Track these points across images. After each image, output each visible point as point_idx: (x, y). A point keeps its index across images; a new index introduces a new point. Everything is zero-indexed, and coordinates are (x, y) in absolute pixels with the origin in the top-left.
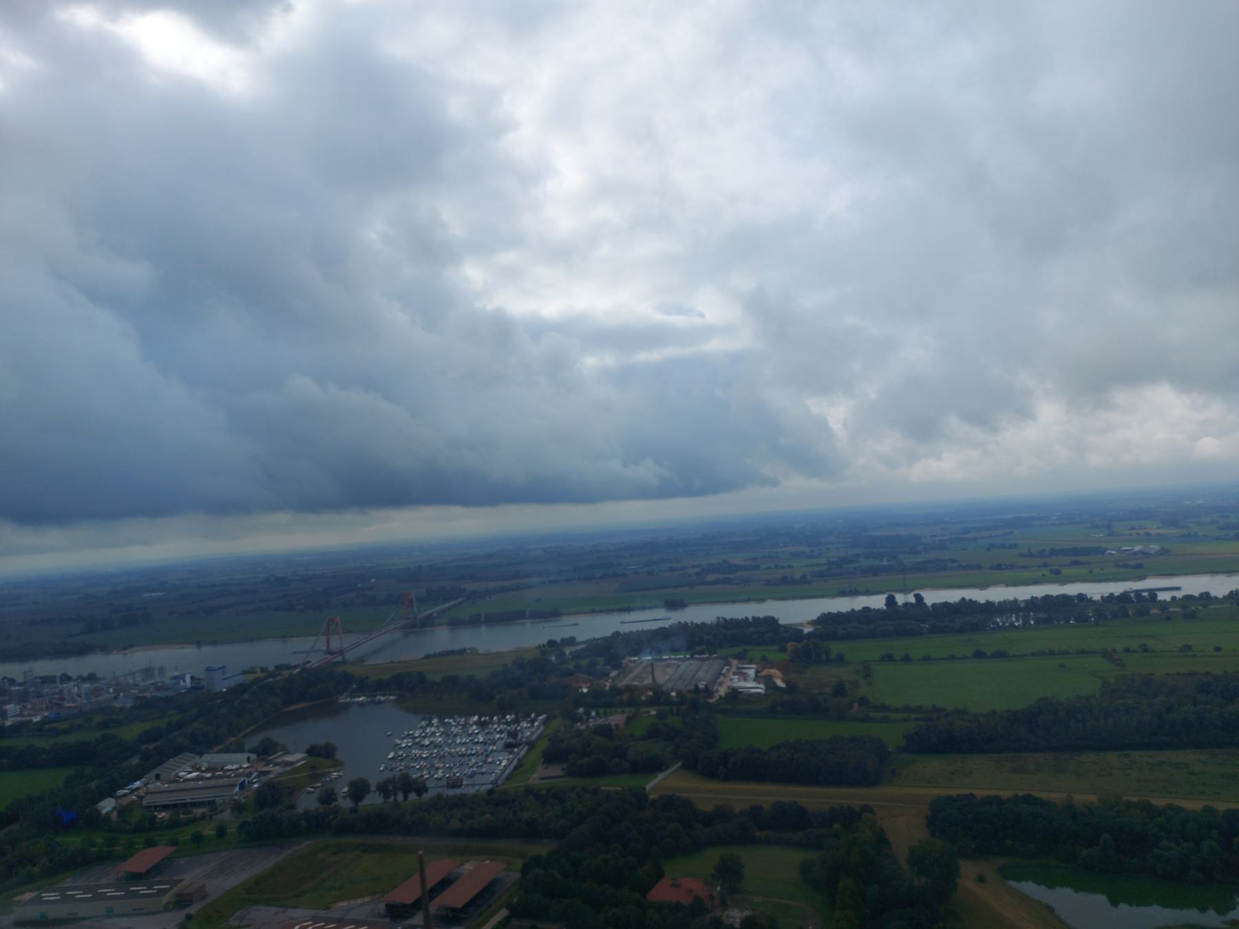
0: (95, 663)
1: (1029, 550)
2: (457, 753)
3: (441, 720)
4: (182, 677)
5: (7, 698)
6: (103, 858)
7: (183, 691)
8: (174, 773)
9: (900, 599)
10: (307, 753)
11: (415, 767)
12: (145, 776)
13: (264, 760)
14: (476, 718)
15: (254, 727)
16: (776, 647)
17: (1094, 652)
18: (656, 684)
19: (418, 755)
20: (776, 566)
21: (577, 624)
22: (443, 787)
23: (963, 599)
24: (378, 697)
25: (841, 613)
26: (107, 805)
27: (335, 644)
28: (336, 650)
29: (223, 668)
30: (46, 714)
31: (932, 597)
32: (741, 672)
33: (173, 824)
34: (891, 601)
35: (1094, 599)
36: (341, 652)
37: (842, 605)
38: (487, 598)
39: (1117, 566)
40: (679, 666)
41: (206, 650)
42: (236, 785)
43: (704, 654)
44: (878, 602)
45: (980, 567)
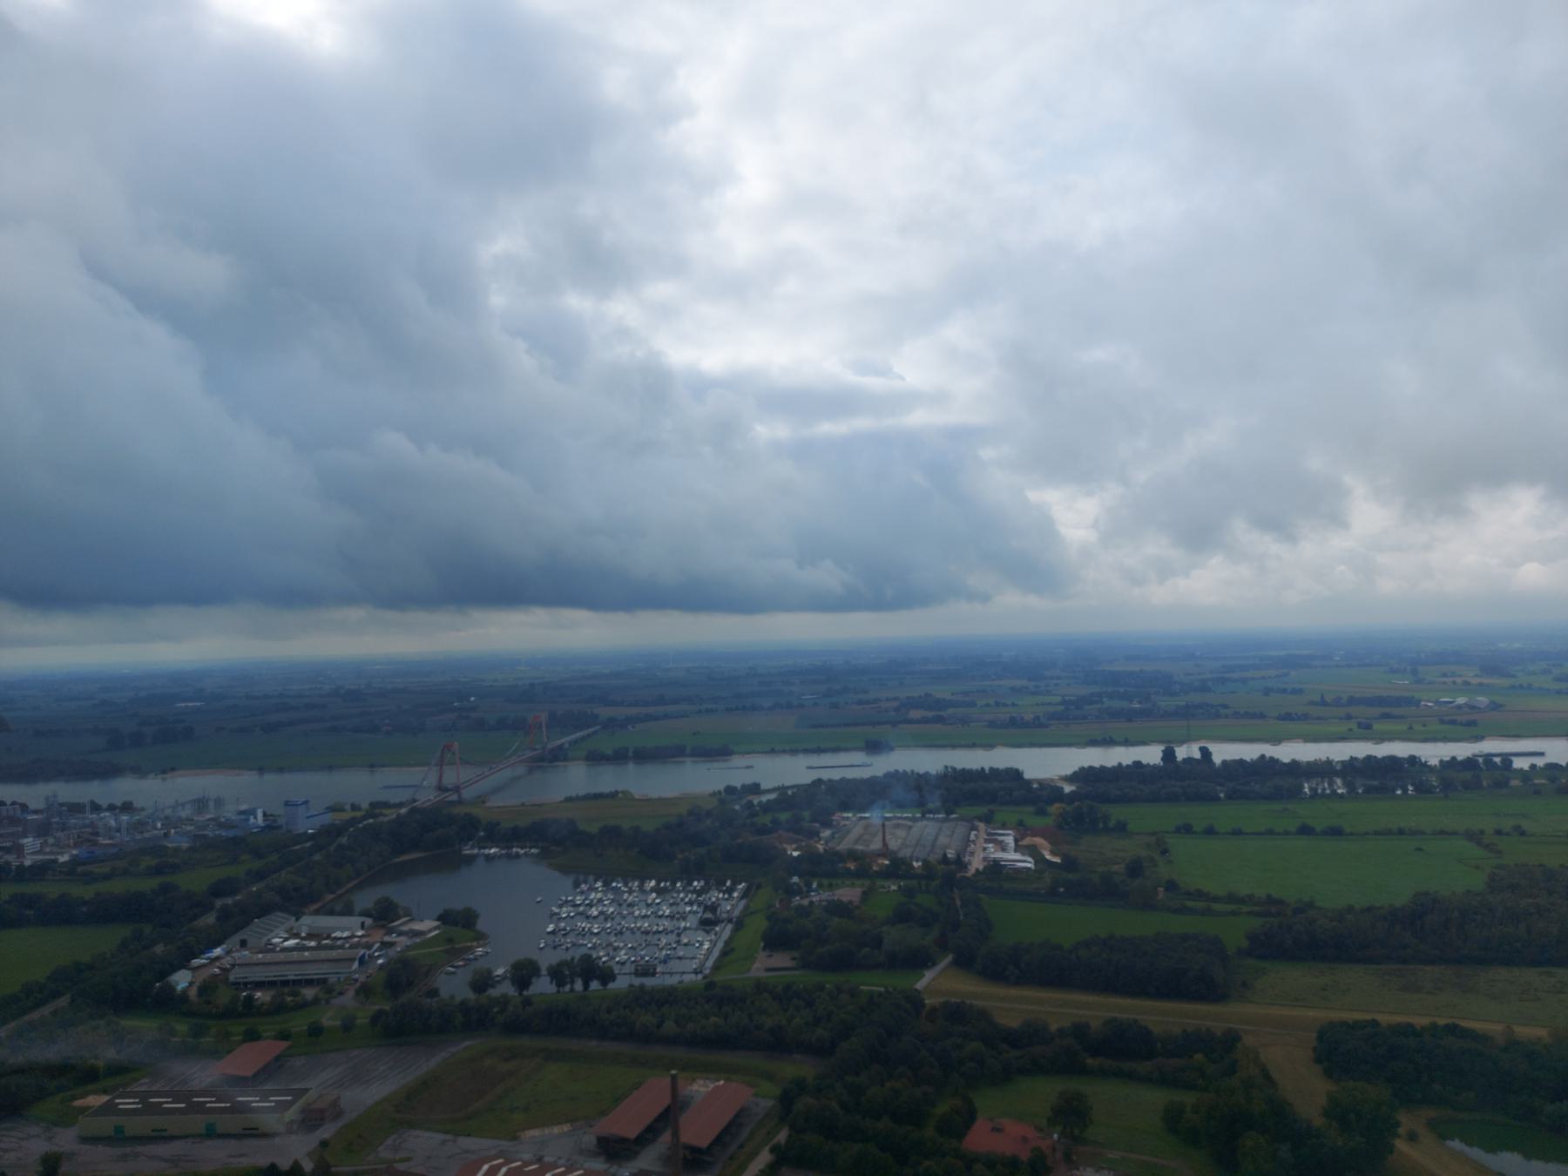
0: (124, 788)
1: (1322, 697)
2: (639, 929)
4: (253, 812)
5: (20, 829)
7: (255, 830)
8: (265, 940)
9: (1181, 753)
10: (438, 919)
11: (586, 945)
12: (227, 942)
13: (383, 927)
14: (653, 883)
15: (355, 882)
16: (1031, 809)
17: (1455, 833)
18: (887, 849)
19: (586, 929)
20: (997, 704)
21: (751, 767)
22: (630, 974)
24: (514, 850)
26: (181, 980)
27: (450, 778)
28: (450, 786)
29: (306, 802)
30: (75, 852)
31: (1222, 753)
32: (996, 839)
33: (277, 1009)
34: (1169, 755)
35: (1429, 764)
36: (457, 789)
38: (630, 727)
39: (1442, 722)
40: (910, 827)
41: (270, 778)
42: (353, 960)
43: (939, 813)
44: (1151, 755)
45: (1262, 716)
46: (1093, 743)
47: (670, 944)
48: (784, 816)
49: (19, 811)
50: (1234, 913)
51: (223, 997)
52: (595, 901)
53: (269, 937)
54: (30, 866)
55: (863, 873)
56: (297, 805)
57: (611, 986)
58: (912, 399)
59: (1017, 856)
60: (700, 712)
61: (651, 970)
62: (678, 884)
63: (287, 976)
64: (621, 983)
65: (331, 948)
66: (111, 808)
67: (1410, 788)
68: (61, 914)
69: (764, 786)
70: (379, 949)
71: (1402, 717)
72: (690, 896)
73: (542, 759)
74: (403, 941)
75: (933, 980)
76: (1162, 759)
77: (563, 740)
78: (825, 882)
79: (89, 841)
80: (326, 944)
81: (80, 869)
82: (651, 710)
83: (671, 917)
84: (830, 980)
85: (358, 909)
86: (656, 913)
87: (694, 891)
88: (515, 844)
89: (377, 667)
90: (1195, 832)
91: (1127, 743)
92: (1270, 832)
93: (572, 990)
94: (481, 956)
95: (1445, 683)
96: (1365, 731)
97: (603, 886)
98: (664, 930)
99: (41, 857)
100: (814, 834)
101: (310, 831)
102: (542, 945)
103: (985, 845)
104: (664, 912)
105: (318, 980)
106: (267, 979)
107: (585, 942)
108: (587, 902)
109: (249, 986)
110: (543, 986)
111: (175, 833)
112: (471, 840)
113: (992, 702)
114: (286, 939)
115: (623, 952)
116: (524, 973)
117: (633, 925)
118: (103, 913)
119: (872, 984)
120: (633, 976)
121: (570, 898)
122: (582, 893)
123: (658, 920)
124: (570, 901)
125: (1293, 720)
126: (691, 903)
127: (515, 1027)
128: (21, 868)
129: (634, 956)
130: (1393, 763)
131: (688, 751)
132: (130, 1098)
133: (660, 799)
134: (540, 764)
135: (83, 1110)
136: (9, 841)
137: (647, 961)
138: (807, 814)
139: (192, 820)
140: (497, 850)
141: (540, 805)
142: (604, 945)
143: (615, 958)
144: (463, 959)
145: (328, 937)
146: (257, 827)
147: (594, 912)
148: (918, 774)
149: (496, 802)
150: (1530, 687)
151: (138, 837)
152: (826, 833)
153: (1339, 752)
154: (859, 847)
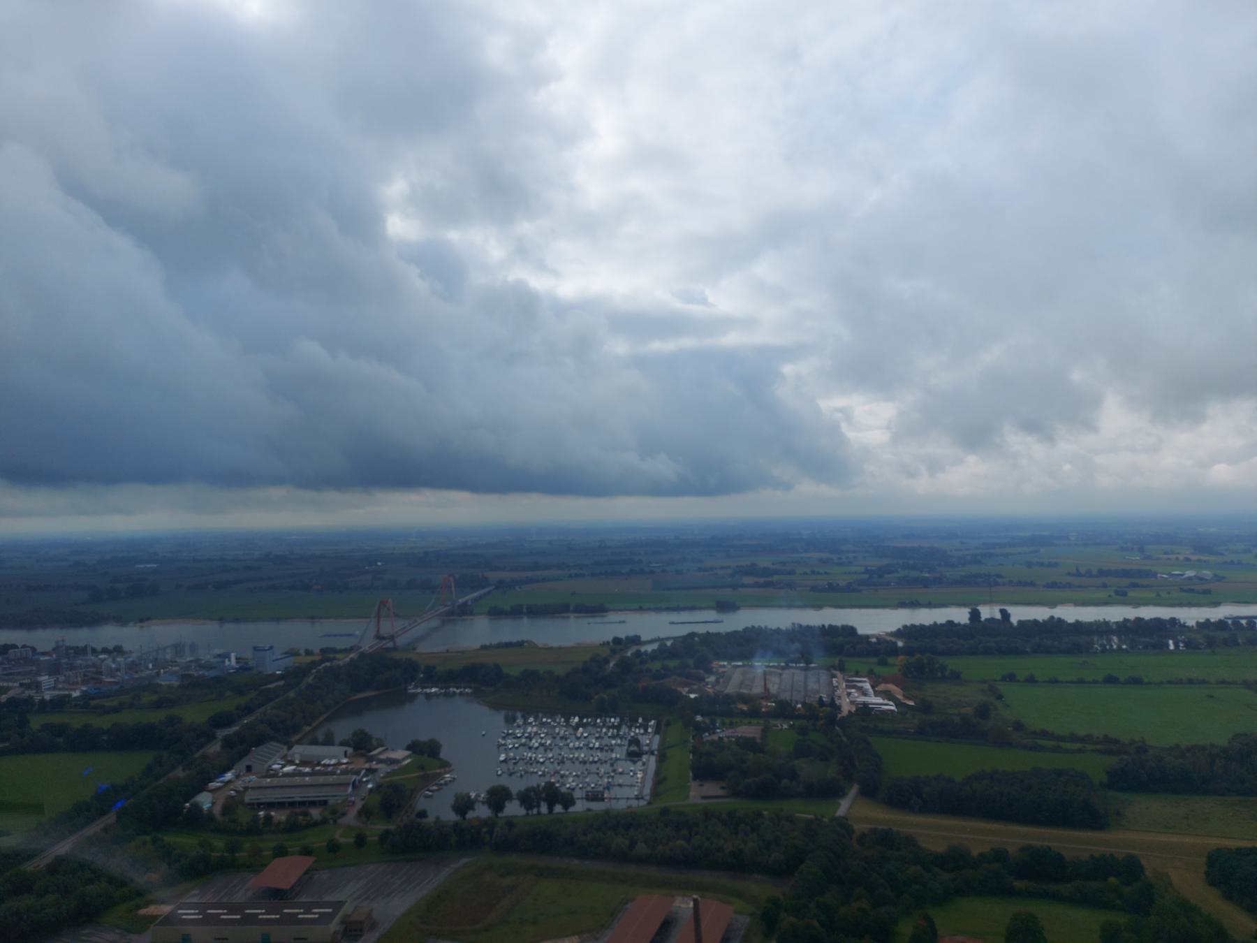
0: (108, 635)
1: (1077, 569)
2: (577, 759)
3: (536, 718)
4: (227, 656)
5: (34, 668)
6: (227, 866)
7: (232, 671)
8: (266, 766)
9: (986, 612)
10: (408, 748)
11: (536, 773)
12: (234, 767)
13: (362, 755)
14: (577, 719)
15: (324, 716)
16: (875, 660)
17: (1235, 683)
18: (769, 692)
19: (533, 759)
20: (813, 572)
21: (624, 622)
22: (582, 798)
23: (1052, 617)
24: (451, 689)
25: (924, 626)
26: (205, 800)
27: (386, 628)
28: (386, 635)
29: (271, 648)
30: (84, 688)
31: (1018, 614)
32: (855, 686)
33: (292, 827)
34: (975, 615)
35: (1187, 624)
36: (392, 638)
37: (926, 617)
38: (517, 588)
39: (1182, 590)
40: (780, 675)
41: (229, 627)
42: (347, 785)
43: (800, 663)
44: (960, 615)
45: (1032, 584)
46: (903, 605)
47: (608, 773)
48: (672, 664)
49: (30, 653)
50: (1080, 751)
51: (244, 817)
52: (533, 734)
53: (269, 763)
54: (51, 700)
55: (754, 713)
56: (266, 650)
57: (571, 809)
58: (726, 323)
59: (879, 700)
60: (570, 576)
61: (600, 796)
62: (598, 721)
63: (293, 798)
64: (579, 807)
65: (326, 774)
66: (105, 651)
67: (1181, 645)
68: (84, 742)
69: (643, 638)
70: (365, 775)
71: (1148, 586)
72: (611, 730)
73: (451, 613)
74: (383, 769)
75: (850, 807)
76: (970, 619)
77: (467, 598)
78: (727, 721)
79: (94, 679)
80: (320, 770)
81: (93, 703)
82: (529, 574)
83: (601, 749)
84: (767, 808)
85: (337, 740)
86: (588, 745)
87: (613, 727)
88: (452, 684)
89: (294, 537)
90: (1019, 681)
91: (930, 605)
92: (1081, 681)
93: (539, 813)
94: (450, 781)
95: (1169, 559)
96: (1121, 597)
97: (535, 721)
98: (599, 760)
99: (57, 693)
100: (701, 679)
101: (278, 672)
102: (499, 773)
103: (849, 691)
104: (594, 744)
105: (320, 801)
106: (277, 801)
107: (535, 770)
108: (526, 735)
109: (262, 806)
110: (513, 809)
111: (165, 673)
112: (413, 681)
113: (808, 571)
114: (284, 766)
115: (571, 780)
116: (498, 798)
117: (571, 756)
118: (126, 741)
119: (804, 811)
120: (585, 801)
121: (510, 731)
122: (519, 726)
123: (591, 752)
124: (511, 734)
125: (1059, 587)
126: (613, 737)
127: (504, 846)
128: (43, 701)
129: (581, 783)
130: (1158, 624)
131: (571, 608)
132: (191, 909)
133: (560, 648)
134: (452, 618)
135: (152, 918)
136: (28, 679)
137: (593, 788)
138: (691, 662)
139: (176, 662)
140: (437, 689)
141: (463, 652)
142: (552, 773)
143: (565, 785)
144: (436, 784)
145: (319, 764)
146: (233, 669)
147: (535, 743)
148: (771, 629)
149: (423, 648)
150: (1240, 563)
151: (136, 676)
152: (712, 679)
153: (1115, 614)
154: (745, 691)
